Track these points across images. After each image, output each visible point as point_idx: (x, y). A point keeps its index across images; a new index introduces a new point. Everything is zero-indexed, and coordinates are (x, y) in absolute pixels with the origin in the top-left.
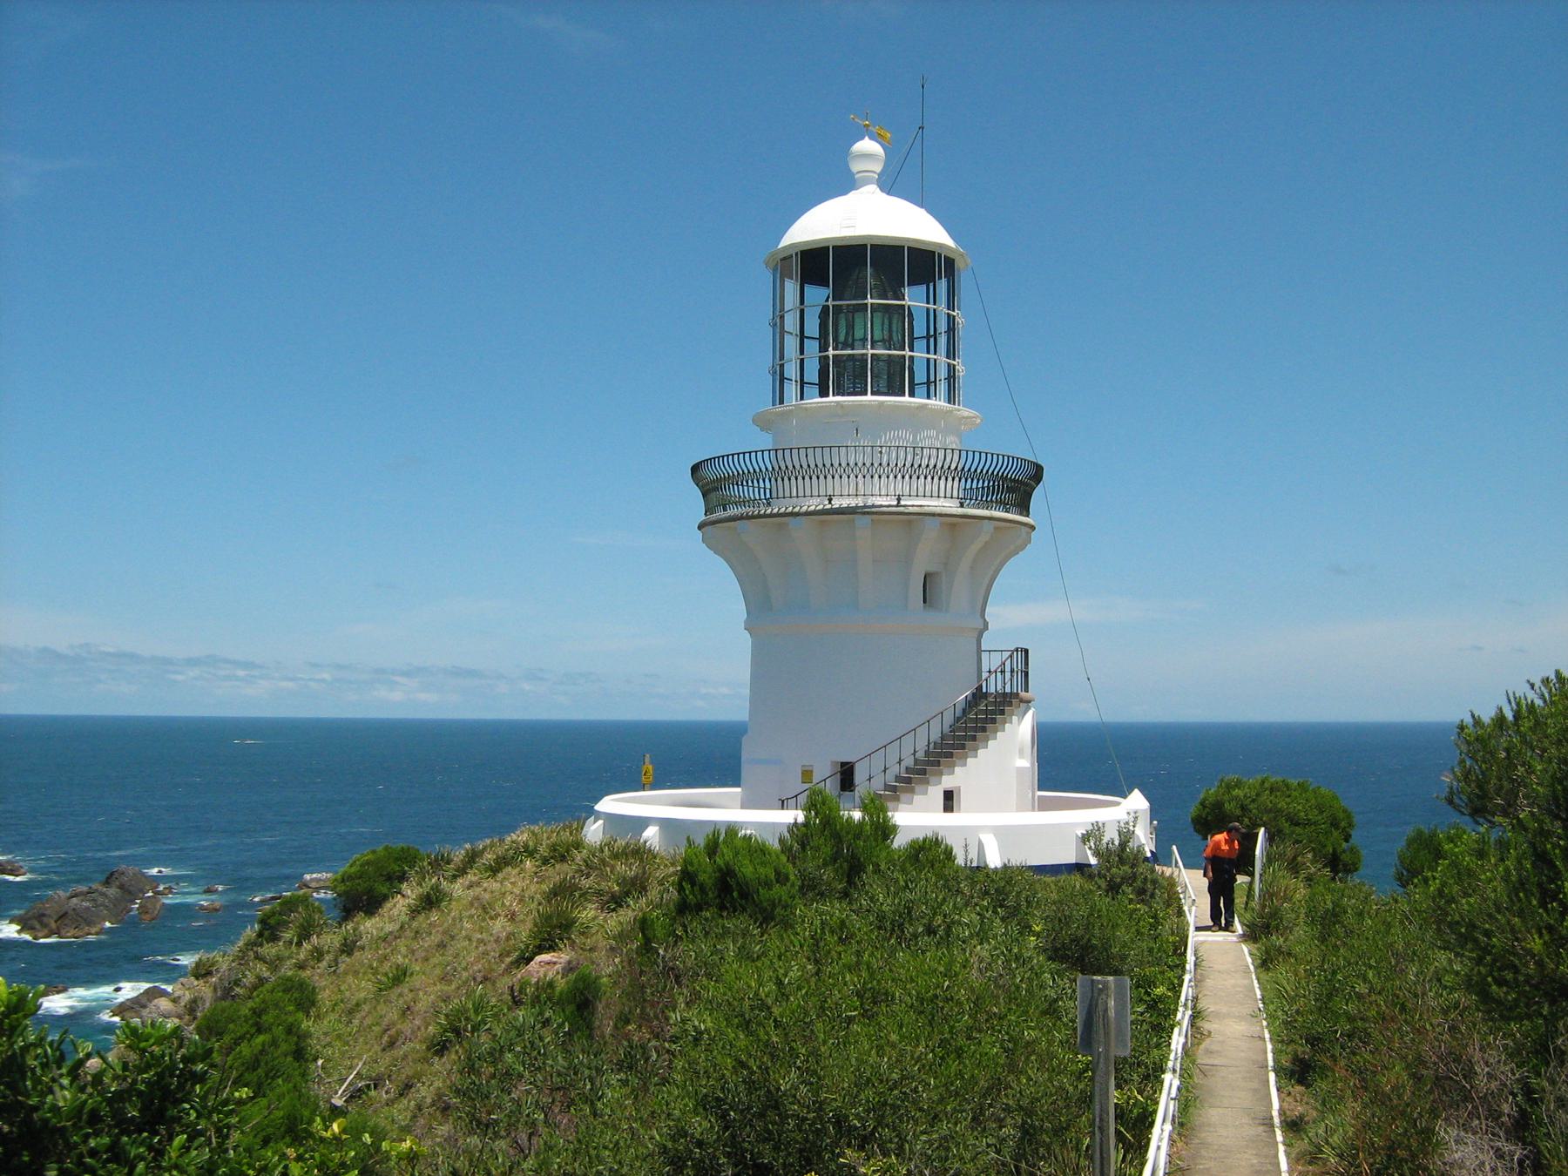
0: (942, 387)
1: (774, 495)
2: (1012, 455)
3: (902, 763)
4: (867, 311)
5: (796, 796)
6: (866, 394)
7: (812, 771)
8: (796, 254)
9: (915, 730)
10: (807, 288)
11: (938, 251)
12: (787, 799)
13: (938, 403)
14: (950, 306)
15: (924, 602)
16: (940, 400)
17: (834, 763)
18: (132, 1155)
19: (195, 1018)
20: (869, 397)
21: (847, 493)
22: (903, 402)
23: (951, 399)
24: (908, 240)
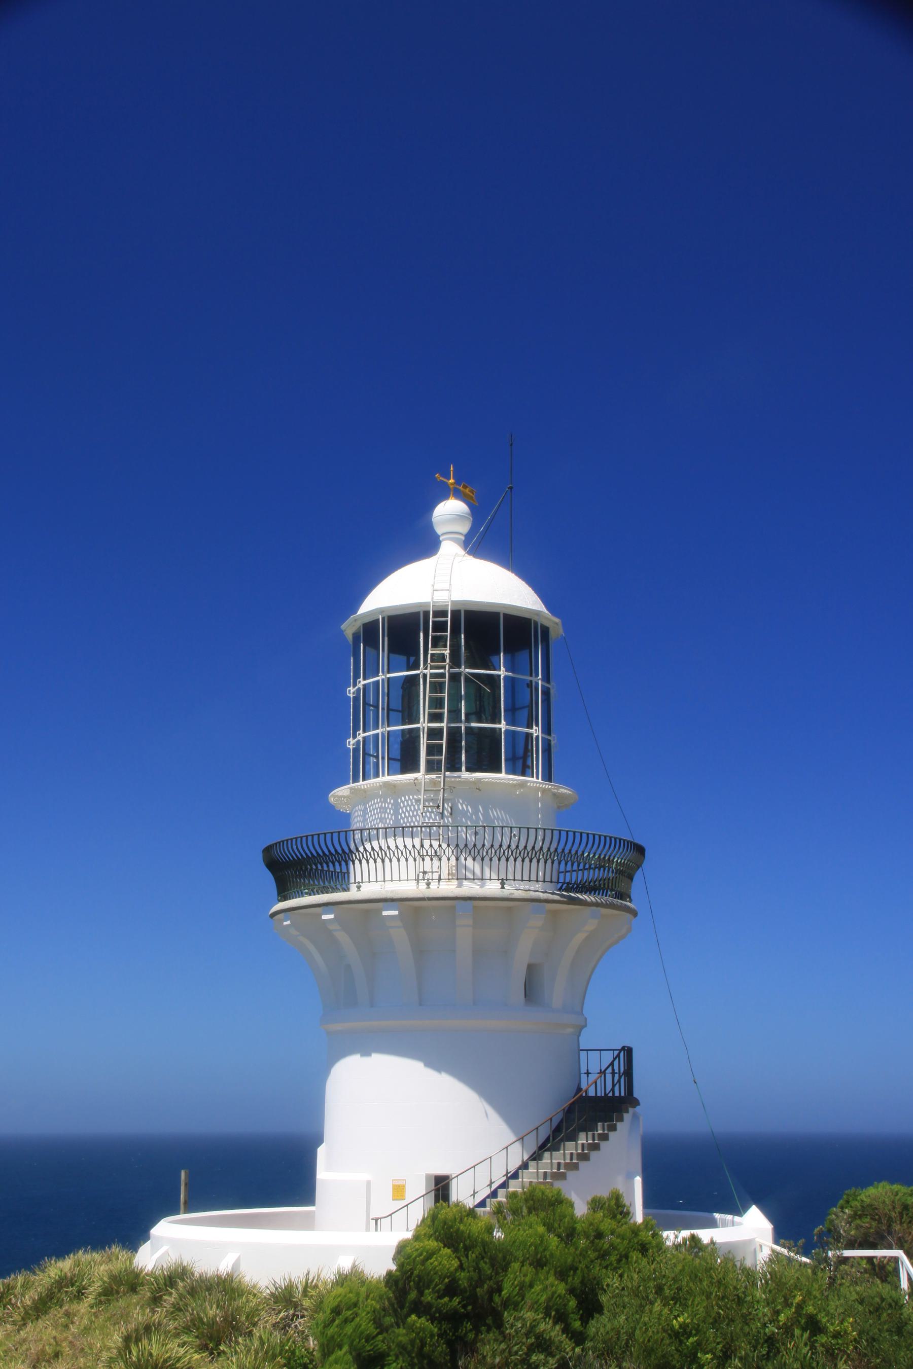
0: (538, 761)
1: (366, 879)
2: (619, 837)
3: (493, 1185)
4: (408, 670)
5: (391, 1215)
6: (460, 770)
7: (404, 1186)
8: (383, 619)
9: (507, 1148)
10: (390, 655)
11: (535, 618)
12: (381, 1218)
13: (534, 779)
14: (547, 678)
15: (525, 997)
16: (538, 778)
17: (428, 1177)
18: (816, 1345)
19: (740, 1269)
20: (503, 776)
21: (549, 880)
22: (501, 779)
23: (548, 777)
24: (504, 606)
